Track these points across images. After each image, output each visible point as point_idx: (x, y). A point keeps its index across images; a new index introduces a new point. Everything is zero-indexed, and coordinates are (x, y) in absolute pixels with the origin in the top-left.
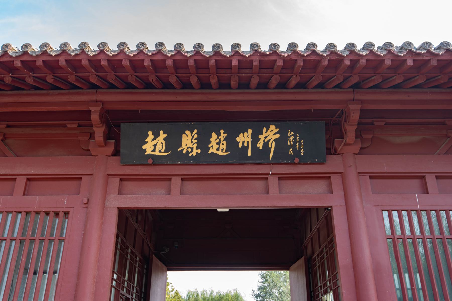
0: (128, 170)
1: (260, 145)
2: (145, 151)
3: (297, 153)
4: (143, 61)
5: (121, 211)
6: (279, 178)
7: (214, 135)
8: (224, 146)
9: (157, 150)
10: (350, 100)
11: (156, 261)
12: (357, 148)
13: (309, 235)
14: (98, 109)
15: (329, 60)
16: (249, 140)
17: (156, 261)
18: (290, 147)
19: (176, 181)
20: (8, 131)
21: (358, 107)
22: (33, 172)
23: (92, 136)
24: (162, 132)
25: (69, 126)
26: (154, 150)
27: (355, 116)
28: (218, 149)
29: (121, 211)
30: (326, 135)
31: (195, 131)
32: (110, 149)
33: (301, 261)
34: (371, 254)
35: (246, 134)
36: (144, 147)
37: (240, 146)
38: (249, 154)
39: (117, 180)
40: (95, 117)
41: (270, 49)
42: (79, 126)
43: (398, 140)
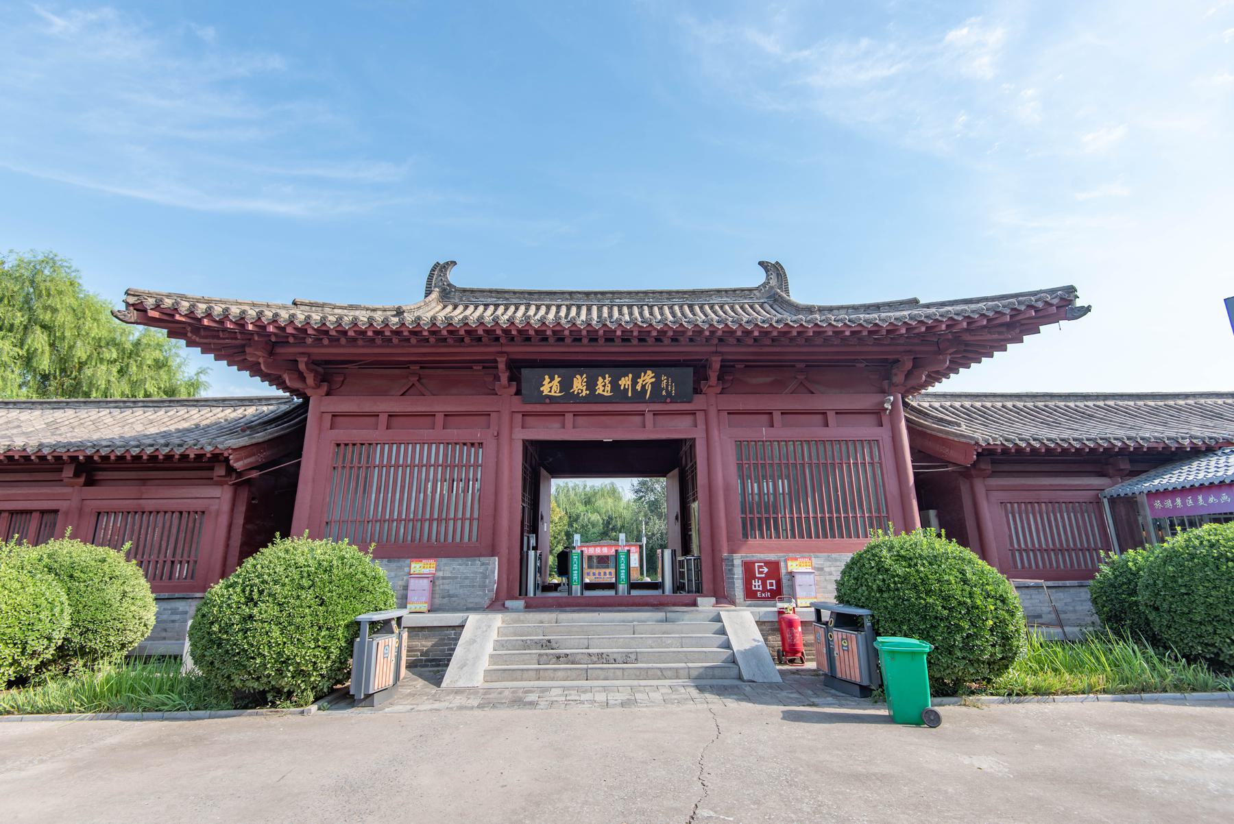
0: (529, 408)
1: (639, 388)
2: (543, 392)
3: (669, 393)
4: (545, 331)
5: (524, 441)
6: (654, 414)
7: (600, 378)
8: (608, 388)
9: (553, 391)
10: (713, 353)
11: (544, 472)
12: (719, 389)
13: (684, 448)
14: (504, 359)
15: (693, 331)
16: (630, 383)
17: (544, 472)
18: (663, 389)
19: (569, 417)
20: (422, 372)
21: (720, 358)
22: (449, 410)
23: (497, 378)
24: (556, 376)
25: (475, 368)
26: (550, 392)
27: (717, 366)
28: (604, 391)
29: (524, 441)
30: (694, 376)
31: (585, 376)
32: (513, 390)
33: (676, 472)
34: (724, 476)
35: (627, 378)
36: (542, 389)
37: (622, 388)
38: (630, 395)
39: (520, 416)
40: (502, 366)
41: (612, 564)
42: (484, 367)
43: (755, 381)
